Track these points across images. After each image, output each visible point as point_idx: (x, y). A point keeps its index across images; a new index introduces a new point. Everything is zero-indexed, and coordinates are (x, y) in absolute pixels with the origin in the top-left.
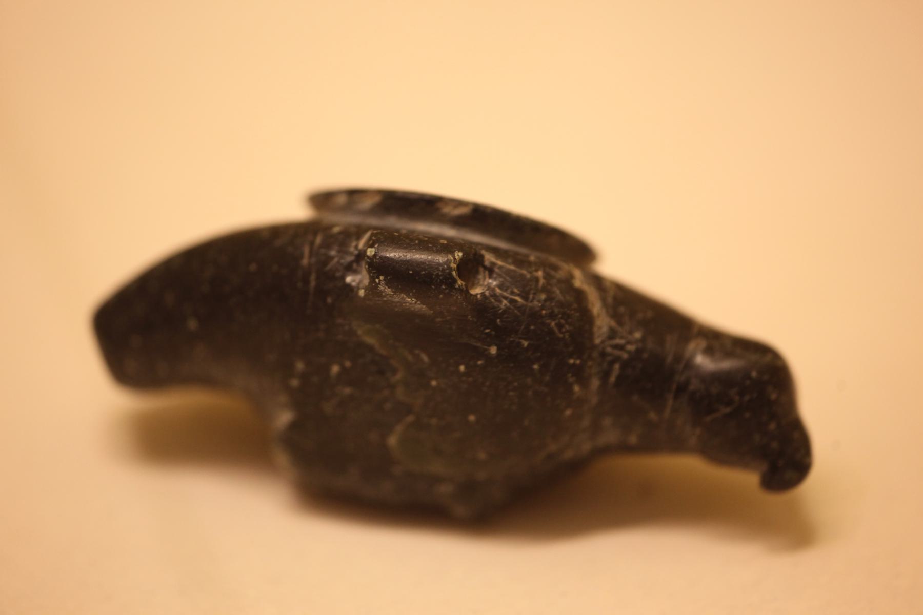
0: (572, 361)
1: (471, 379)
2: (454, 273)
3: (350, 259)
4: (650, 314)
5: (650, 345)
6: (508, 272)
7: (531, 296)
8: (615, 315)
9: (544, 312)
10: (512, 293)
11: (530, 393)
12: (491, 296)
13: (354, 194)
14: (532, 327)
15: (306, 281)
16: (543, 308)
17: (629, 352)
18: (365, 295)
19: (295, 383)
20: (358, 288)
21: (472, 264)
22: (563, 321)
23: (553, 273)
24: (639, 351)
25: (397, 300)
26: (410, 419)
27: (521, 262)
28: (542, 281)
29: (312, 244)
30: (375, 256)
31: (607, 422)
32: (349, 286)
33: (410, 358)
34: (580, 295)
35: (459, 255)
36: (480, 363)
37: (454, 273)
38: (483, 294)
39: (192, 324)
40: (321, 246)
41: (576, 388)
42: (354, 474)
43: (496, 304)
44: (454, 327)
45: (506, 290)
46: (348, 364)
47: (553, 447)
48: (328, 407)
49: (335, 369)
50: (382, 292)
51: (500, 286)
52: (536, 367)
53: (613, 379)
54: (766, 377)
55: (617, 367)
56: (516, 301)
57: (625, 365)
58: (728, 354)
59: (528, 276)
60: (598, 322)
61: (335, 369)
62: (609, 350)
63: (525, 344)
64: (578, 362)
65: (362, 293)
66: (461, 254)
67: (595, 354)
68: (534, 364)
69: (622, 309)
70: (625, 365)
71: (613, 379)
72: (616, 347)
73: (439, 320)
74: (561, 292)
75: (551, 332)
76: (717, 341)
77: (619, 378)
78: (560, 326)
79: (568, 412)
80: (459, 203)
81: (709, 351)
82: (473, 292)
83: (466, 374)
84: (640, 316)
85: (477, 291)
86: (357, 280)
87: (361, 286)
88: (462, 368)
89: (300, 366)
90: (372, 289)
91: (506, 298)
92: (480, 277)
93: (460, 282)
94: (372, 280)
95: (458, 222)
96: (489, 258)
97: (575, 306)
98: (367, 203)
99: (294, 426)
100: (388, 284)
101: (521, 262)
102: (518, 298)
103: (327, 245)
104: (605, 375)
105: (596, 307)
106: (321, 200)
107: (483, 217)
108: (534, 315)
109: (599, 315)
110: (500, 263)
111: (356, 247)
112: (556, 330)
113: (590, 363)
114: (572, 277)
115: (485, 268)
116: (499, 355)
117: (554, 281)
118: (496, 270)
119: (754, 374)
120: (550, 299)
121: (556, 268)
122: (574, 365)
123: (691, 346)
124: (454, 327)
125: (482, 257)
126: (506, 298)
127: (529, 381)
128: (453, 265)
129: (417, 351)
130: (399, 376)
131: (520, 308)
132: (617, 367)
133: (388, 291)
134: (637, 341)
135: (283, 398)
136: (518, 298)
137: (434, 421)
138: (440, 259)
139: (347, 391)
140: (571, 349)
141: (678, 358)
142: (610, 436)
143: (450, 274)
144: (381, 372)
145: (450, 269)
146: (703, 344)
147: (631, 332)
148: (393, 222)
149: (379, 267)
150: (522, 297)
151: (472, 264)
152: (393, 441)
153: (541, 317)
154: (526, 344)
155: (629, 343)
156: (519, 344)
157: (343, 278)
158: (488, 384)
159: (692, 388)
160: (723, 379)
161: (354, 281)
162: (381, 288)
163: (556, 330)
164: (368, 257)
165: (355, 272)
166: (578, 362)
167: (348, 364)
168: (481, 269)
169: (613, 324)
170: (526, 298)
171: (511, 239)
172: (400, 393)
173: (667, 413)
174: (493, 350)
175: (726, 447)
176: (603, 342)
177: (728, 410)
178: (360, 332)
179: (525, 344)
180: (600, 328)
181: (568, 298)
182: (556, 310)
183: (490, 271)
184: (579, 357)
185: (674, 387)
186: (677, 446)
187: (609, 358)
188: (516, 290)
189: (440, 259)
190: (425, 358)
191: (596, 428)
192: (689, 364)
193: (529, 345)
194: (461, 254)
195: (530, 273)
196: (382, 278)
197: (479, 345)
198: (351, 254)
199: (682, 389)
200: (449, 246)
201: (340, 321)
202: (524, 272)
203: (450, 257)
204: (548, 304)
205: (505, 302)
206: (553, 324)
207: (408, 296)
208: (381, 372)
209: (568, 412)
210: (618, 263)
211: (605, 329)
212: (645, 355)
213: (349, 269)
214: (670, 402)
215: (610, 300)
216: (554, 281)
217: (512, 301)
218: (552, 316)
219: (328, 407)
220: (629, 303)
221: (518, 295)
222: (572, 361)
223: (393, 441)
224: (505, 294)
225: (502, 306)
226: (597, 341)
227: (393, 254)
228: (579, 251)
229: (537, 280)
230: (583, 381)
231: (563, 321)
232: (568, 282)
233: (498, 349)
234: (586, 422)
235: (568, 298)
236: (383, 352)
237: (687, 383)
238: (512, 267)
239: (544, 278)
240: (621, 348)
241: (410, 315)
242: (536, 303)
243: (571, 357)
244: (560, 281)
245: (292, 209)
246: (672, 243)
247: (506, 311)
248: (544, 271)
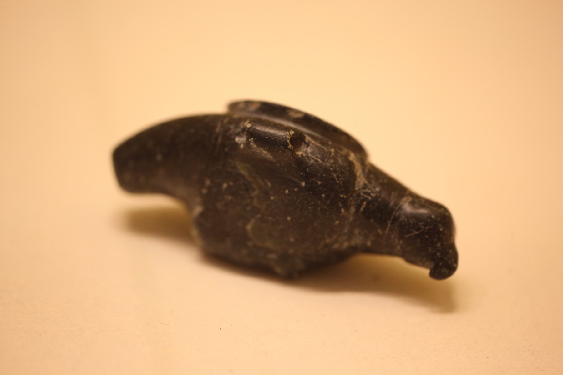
0: (342, 196)
1: (290, 198)
4: (386, 181)
5: (383, 195)
6: (317, 146)
7: (326, 160)
8: (368, 178)
9: (331, 169)
10: (317, 157)
11: (319, 209)
13: (248, 103)
14: (324, 175)
15: (216, 139)
16: (331, 166)
17: (372, 197)
18: (244, 147)
19: (205, 191)
20: (241, 144)
21: (298, 140)
22: (340, 175)
23: (339, 151)
24: (376, 197)
25: (258, 151)
26: (259, 216)
28: (333, 154)
30: (250, 128)
33: (262, 183)
34: (351, 164)
35: (292, 132)
36: (296, 189)
37: (288, 141)
38: (302, 155)
39: (159, 157)
41: (343, 210)
42: (230, 247)
43: (308, 161)
44: (285, 170)
45: (314, 155)
46: (231, 183)
47: (328, 241)
48: (219, 206)
49: (225, 186)
50: (251, 146)
51: (312, 153)
52: (323, 195)
53: (362, 209)
54: (439, 219)
55: (365, 203)
56: (318, 161)
57: (369, 203)
59: (326, 150)
60: (358, 180)
61: (225, 186)
62: (362, 194)
63: (320, 183)
64: (345, 197)
65: (242, 146)
66: (293, 132)
67: (354, 195)
68: (322, 194)
69: (372, 176)
70: (369, 203)
71: (362, 209)
72: (365, 193)
73: (278, 165)
74: (342, 161)
75: (333, 179)
76: (417, 200)
77: (365, 209)
78: (338, 177)
79: (337, 222)
80: (298, 112)
81: (412, 203)
82: (297, 153)
83: (289, 195)
84: (381, 181)
85: (299, 153)
86: (240, 140)
88: (287, 191)
89: (208, 182)
90: (247, 144)
91: (313, 159)
92: (302, 147)
93: (290, 146)
96: (308, 138)
97: (348, 169)
98: (253, 108)
100: (255, 142)
101: (323, 143)
102: (319, 160)
103: (230, 123)
104: (358, 207)
105: (359, 172)
106: (234, 106)
107: (309, 120)
108: (326, 170)
109: (359, 176)
110: (313, 142)
112: (336, 179)
113: (351, 199)
115: (305, 143)
116: (306, 187)
117: (339, 155)
118: (311, 144)
119: (433, 217)
120: (335, 163)
122: (343, 198)
123: (404, 199)
124: (285, 170)
125: (304, 137)
126: (313, 159)
127: (319, 202)
129: (266, 180)
130: (256, 193)
131: (320, 166)
132: (365, 203)
133: (255, 146)
134: (377, 192)
135: (198, 200)
136: (319, 160)
137: (270, 218)
138: (281, 133)
139: (230, 198)
140: (342, 189)
141: (396, 204)
142: (357, 240)
143: (286, 141)
144: (247, 190)
145: (287, 138)
146: (410, 199)
147: (374, 188)
148: (264, 117)
149: (251, 133)
150: (321, 160)
151: (298, 140)
152: (249, 227)
153: (330, 171)
155: (372, 192)
156: (316, 183)
157: (234, 139)
158: (298, 201)
159: (401, 219)
160: (418, 218)
161: (239, 141)
163: (336, 179)
166: (345, 197)
167: (231, 183)
168: (303, 143)
169: (366, 182)
170: (323, 161)
171: (322, 134)
172: (255, 202)
173: (387, 231)
174: (303, 184)
176: (359, 190)
177: (418, 233)
178: (239, 167)
179: (320, 183)
180: (359, 182)
181: (344, 164)
182: (338, 169)
184: (346, 195)
185: (392, 218)
186: (391, 253)
187: (362, 198)
188: (319, 156)
189: (281, 133)
190: (269, 184)
191: (351, 235)
193: (321, 184)
194: (293, 132)
195: (328, 149)
196: (252, 139)
197: (296, 180)
199: (396, 219)
200: (287, 129)
201: (230, 160)
202: (325, 148)
203: (288, 133)
204: (334, 165)
205: (312, 161)
206: (335, 175)
207: (264, 150)
208: (247, 190)
209: (337, 222)
211: (362, 184)
212: (380, 200)
213: (238, 134)
214: (389, 225)
215: (366, 171)
216: (339, 155)
217: (316, 161)
218: (335, 171)
219: (219, 206)
220: (376, 175)
221: (320, 158)
222: (342, 196)
224: (313, 157)
226: (357, 189)
227: (259, 128)
228: (358, 148)
229: (330, 153)
230: (347, 208)
231: (340, 175)
232: (346, 157)
233: (306, 184)
234: (346, 231)
235: (344, 164)
236: (249, 179)
237: (399, 217)
238: (319, 145)
239: (334, 152)
240: (368, 194)
241: (264, 161)
242: (328, 164)
243: (342, 194)
244: (342, 156)
245: (218, 107)
246: (404, 151)
247: (312, 165)
248: (335, 150)
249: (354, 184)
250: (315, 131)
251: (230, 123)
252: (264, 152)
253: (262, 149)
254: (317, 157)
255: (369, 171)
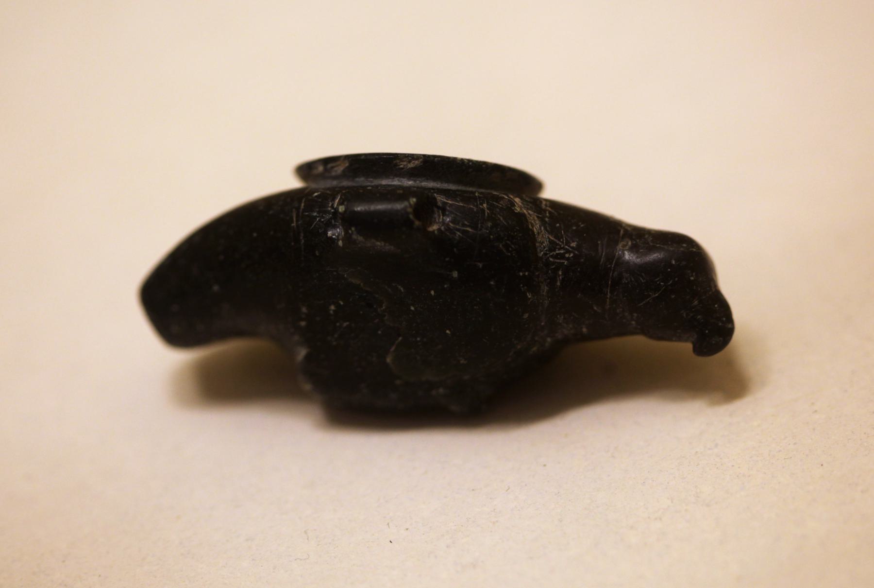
2: (411, 216)
3: (328, 216)
8: (553, 231)
10: (464, 225)
12: (446, 230)
13: (328, 162)
17: (568, 259)
18: (343, 245)
21: (426, 206)
25: (369, 245)
27: (467, 198)
28: (487, 211)
29: (298, 209)
31: (560, 319)
32: (331, 238)
35: (413, 200)
38: (439, 230)
40: (304, 211)
45: (458, 224)
51: (452, 222)
54: (684, 263)
56: (468, 231)
58: (651, 249)
65: (340, 243)
66: (414, 200)
72: (556, 257)
79: (526, 316)
81: (634, 249)
82: (430, 229)
87: (340, 237)
88: (432, 293)
90: (348, 238)
91: (458, 230)
93: (417, 223)
94: (346, 232)
95: (413, 174)
96: (440, 199)
98: (340, 169)
99: (308, 358)
101: (467, 198)
103: (310, 207)
105: (536, 226)
106: (305, 170)
111: (332, 207)
114: (513, 204)
115: (438, 207)
121: (498, 199)
123: (620, 246)
125: (435, 199)
126: (458, 230)
128: (410, 210)
133: (360, 238)
138: (398, 206)
147: (568, 243)
148: (361, 181)
149: (350, 220)
150: (472, 228)
151: (426, 206)
154: (481, 265)
155: (568, 252)
162: (354, 237)
164: (340, 213)
165: (335, 227)
168: (435, 209)
170: (475, 228)
171: (459, 182)
174: (455, 274)
175: (662, 327)
176: (545, 254)
183: (443, 210)
186: (624, 331)
189: (398, 206)
192: (620, 262)
194: (414, 200)
195: (477, 206)
196: (353, 229)
198: (329, 212)
200: (405, 194)
203: (406, 203)
209: (526, 316)
210: (553, 191)
213: (329, 225)
214: (609, 295)
217: (464, 232)
221: (469, 226)
223: (389, 360)
225: (457, 237)
228: (524, 183)
229: (483, 211)
233: (459, 273)
240: (562, 256)
249: (535, 248)
250: (448, 181)
251: (310, 207)
252: (379, 243)
253: (373, 240)
254: (464, 225)
255: (551, 216)
